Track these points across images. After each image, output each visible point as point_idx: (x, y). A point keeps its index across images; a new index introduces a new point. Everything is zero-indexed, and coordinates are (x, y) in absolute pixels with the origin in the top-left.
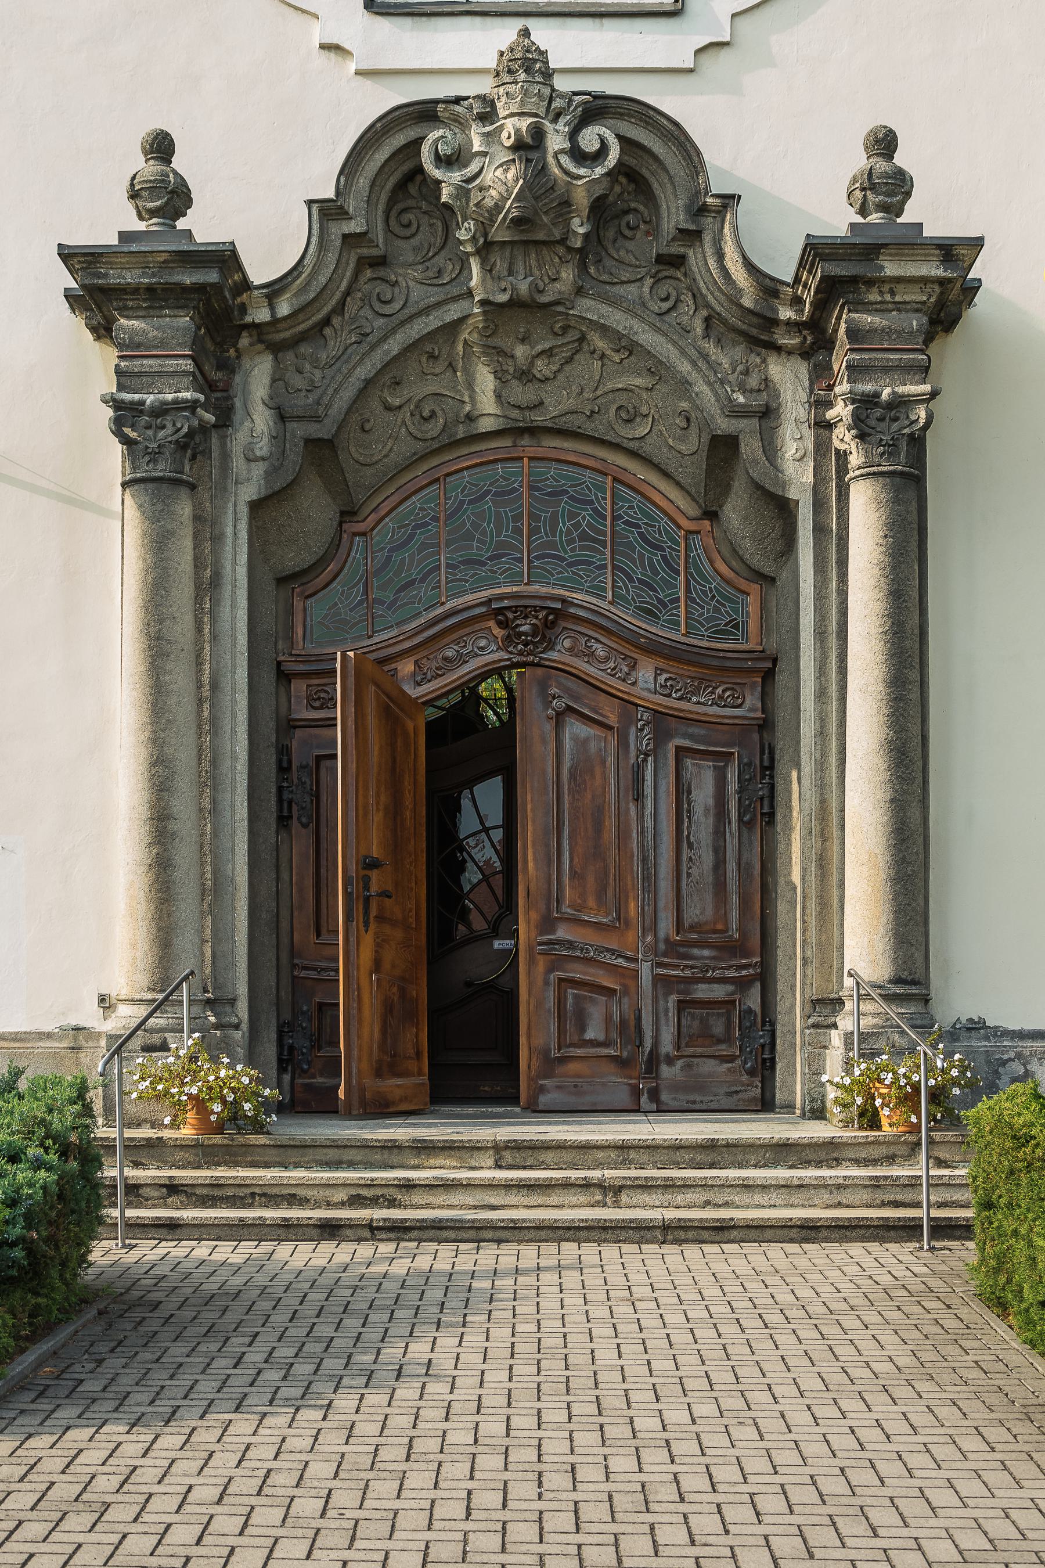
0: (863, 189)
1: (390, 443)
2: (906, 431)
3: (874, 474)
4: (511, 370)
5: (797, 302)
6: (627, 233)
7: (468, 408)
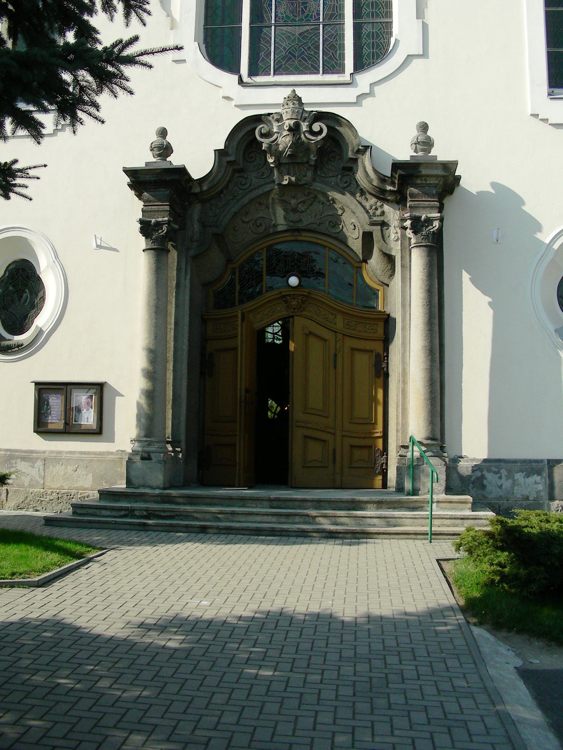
0: (415, 144)
1: (245, 235)
2: (432, 230)
3: (420, 246)
4: (290, 208)
5: (393, 184)
6: (332, 159)
7: (274, 222)
